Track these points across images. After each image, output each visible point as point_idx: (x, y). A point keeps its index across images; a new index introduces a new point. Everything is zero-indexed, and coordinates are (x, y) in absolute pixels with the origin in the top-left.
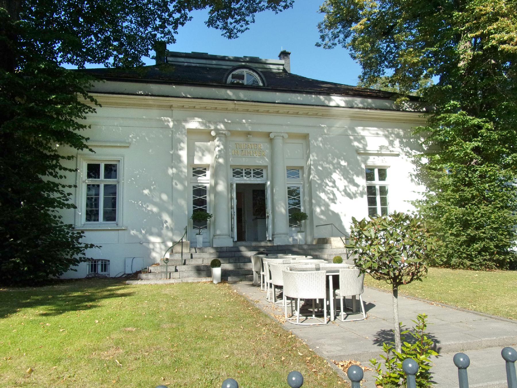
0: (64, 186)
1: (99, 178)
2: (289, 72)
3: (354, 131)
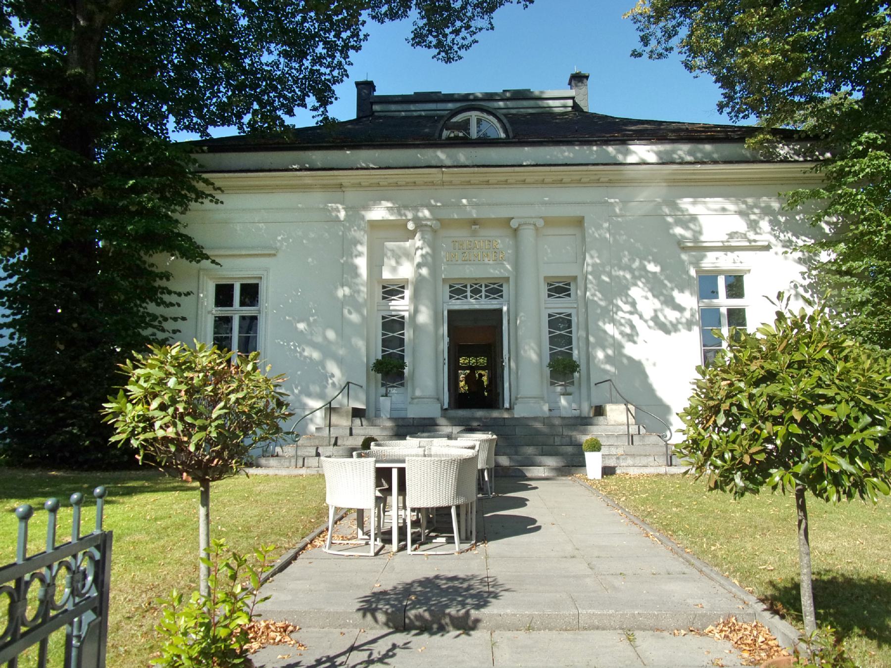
0: (166, 319)
1: (231, 305)
2: (585, 110)
3: (674, 206)
